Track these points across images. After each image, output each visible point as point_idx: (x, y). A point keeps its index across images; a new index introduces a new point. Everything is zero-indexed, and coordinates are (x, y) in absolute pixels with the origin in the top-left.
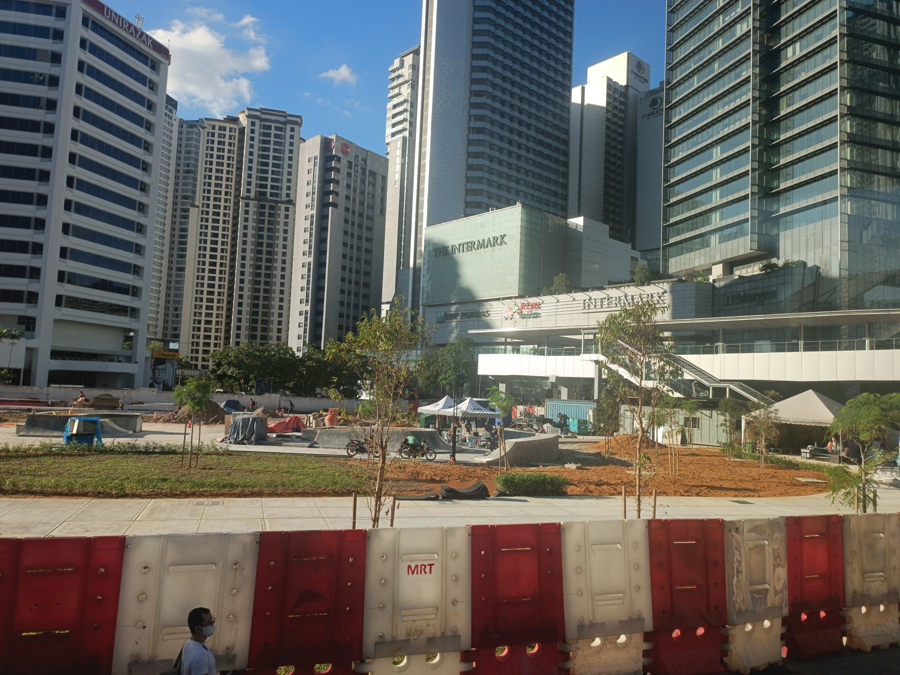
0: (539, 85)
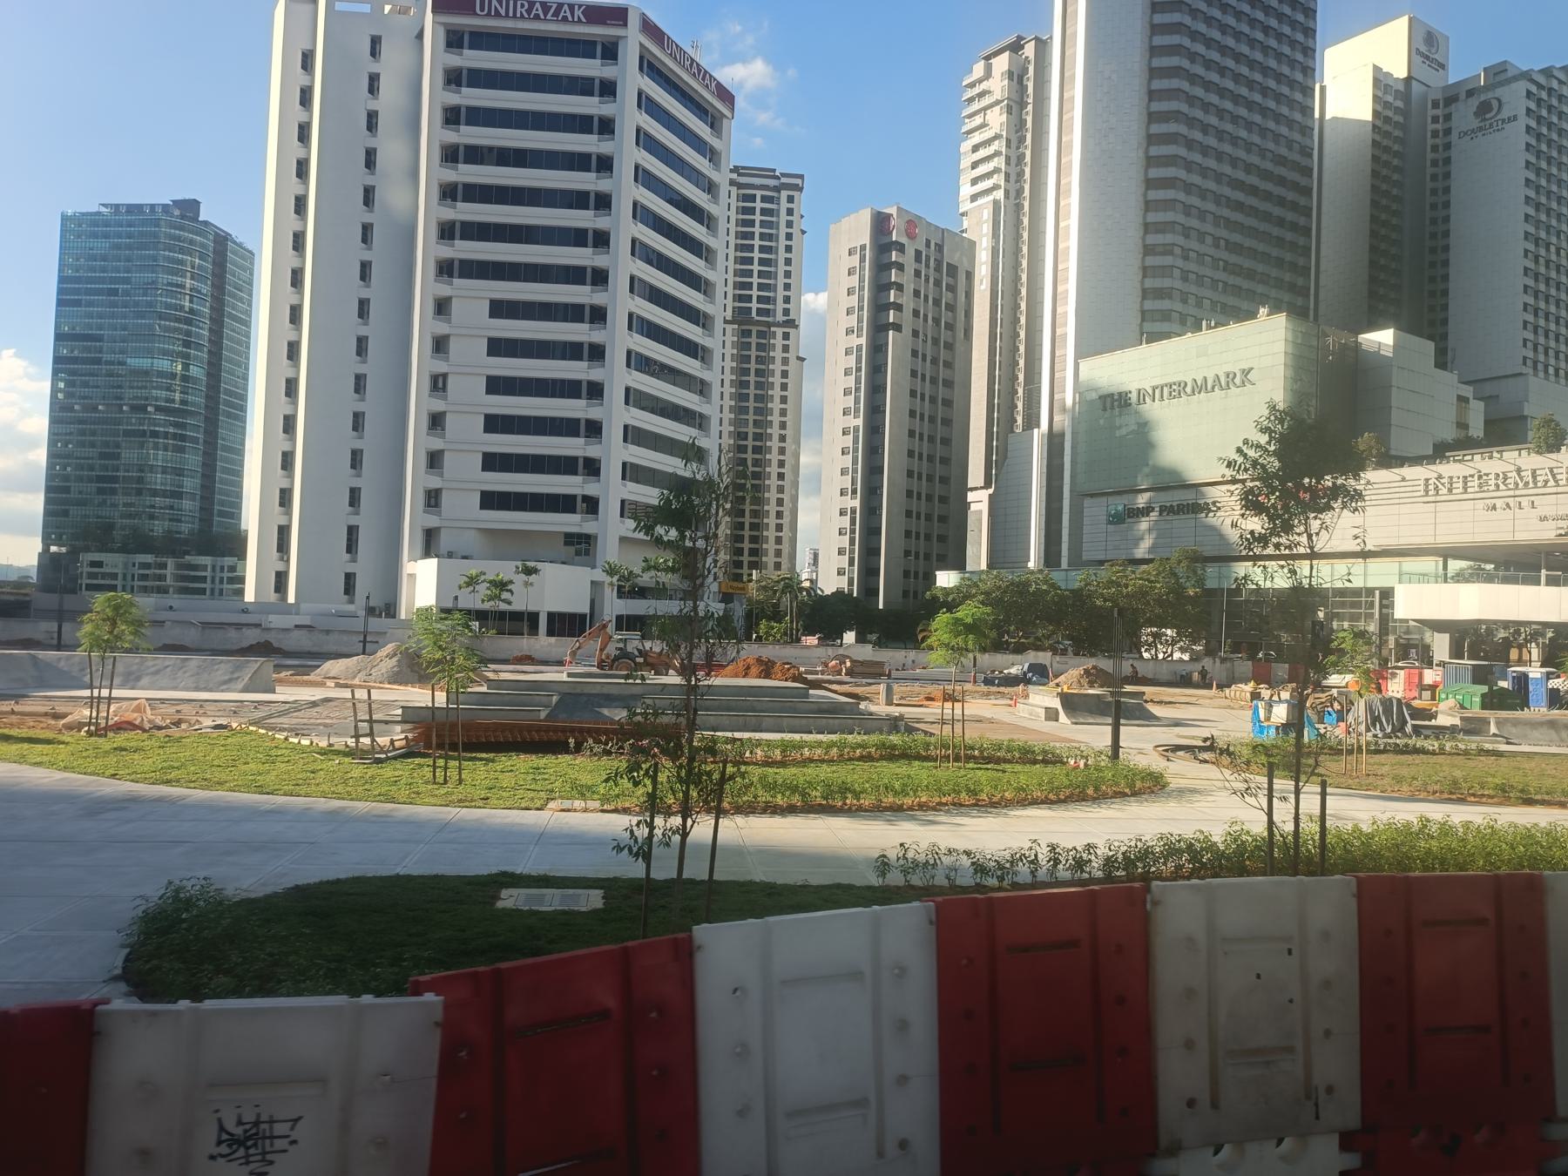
0: (1265, 91)
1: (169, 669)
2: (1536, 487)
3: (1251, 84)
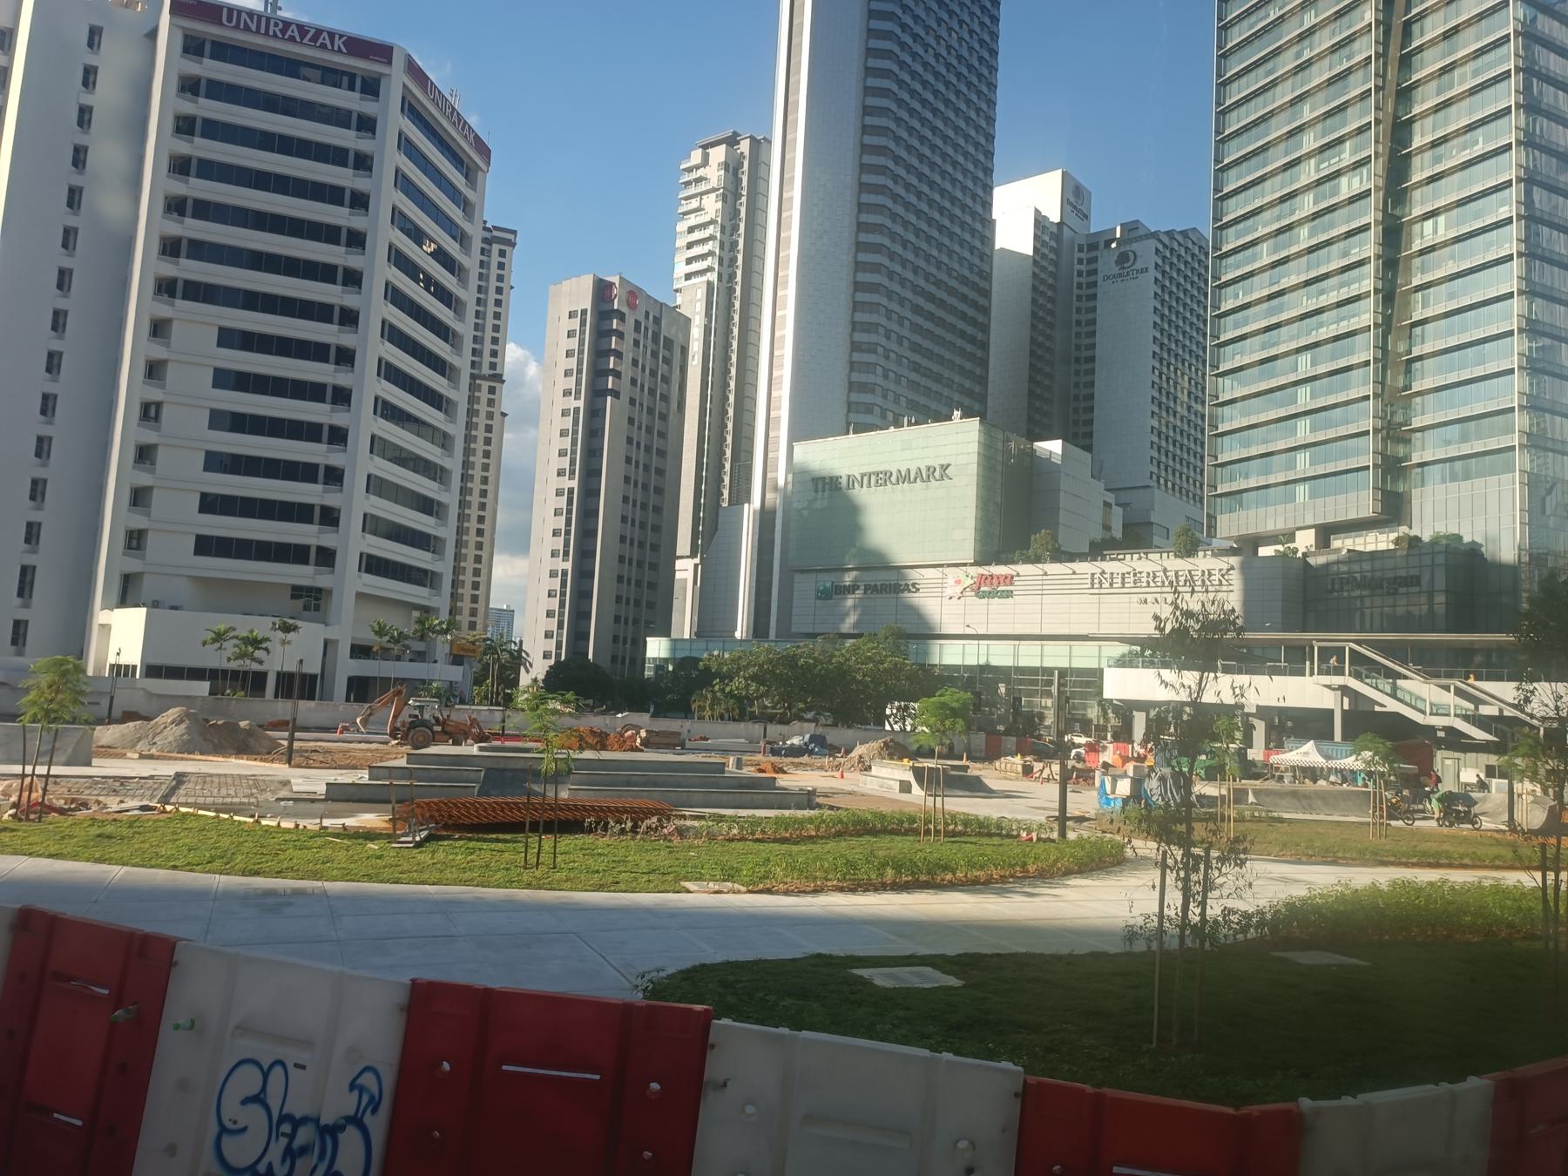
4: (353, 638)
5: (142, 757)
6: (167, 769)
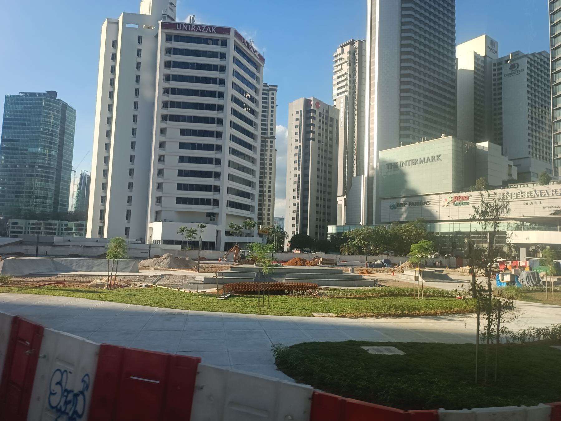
1: (103, 264)
2: (541, 197)
3: (434, 57)
4: (226, 229)
5: (155, 269)
6: (159, 273)
